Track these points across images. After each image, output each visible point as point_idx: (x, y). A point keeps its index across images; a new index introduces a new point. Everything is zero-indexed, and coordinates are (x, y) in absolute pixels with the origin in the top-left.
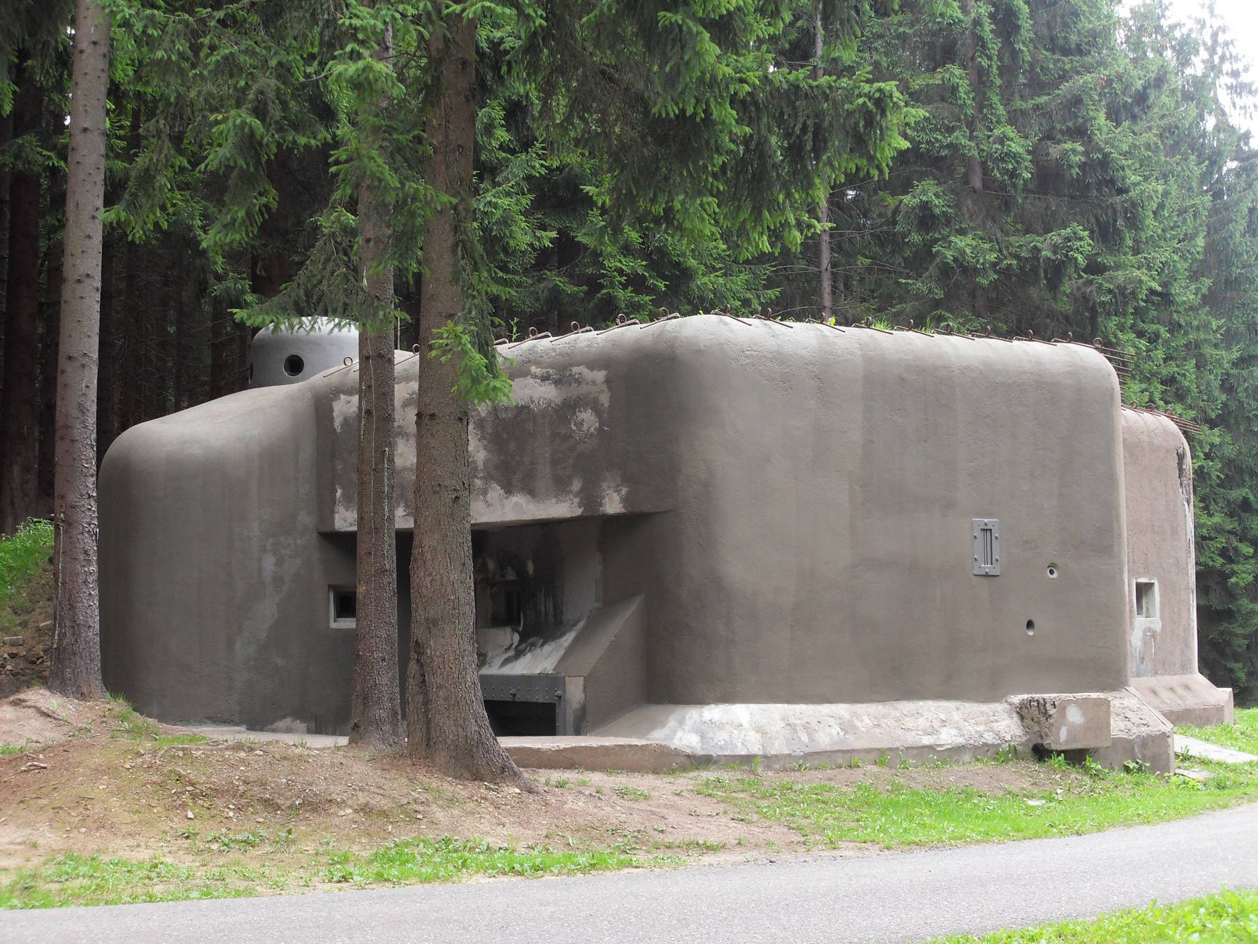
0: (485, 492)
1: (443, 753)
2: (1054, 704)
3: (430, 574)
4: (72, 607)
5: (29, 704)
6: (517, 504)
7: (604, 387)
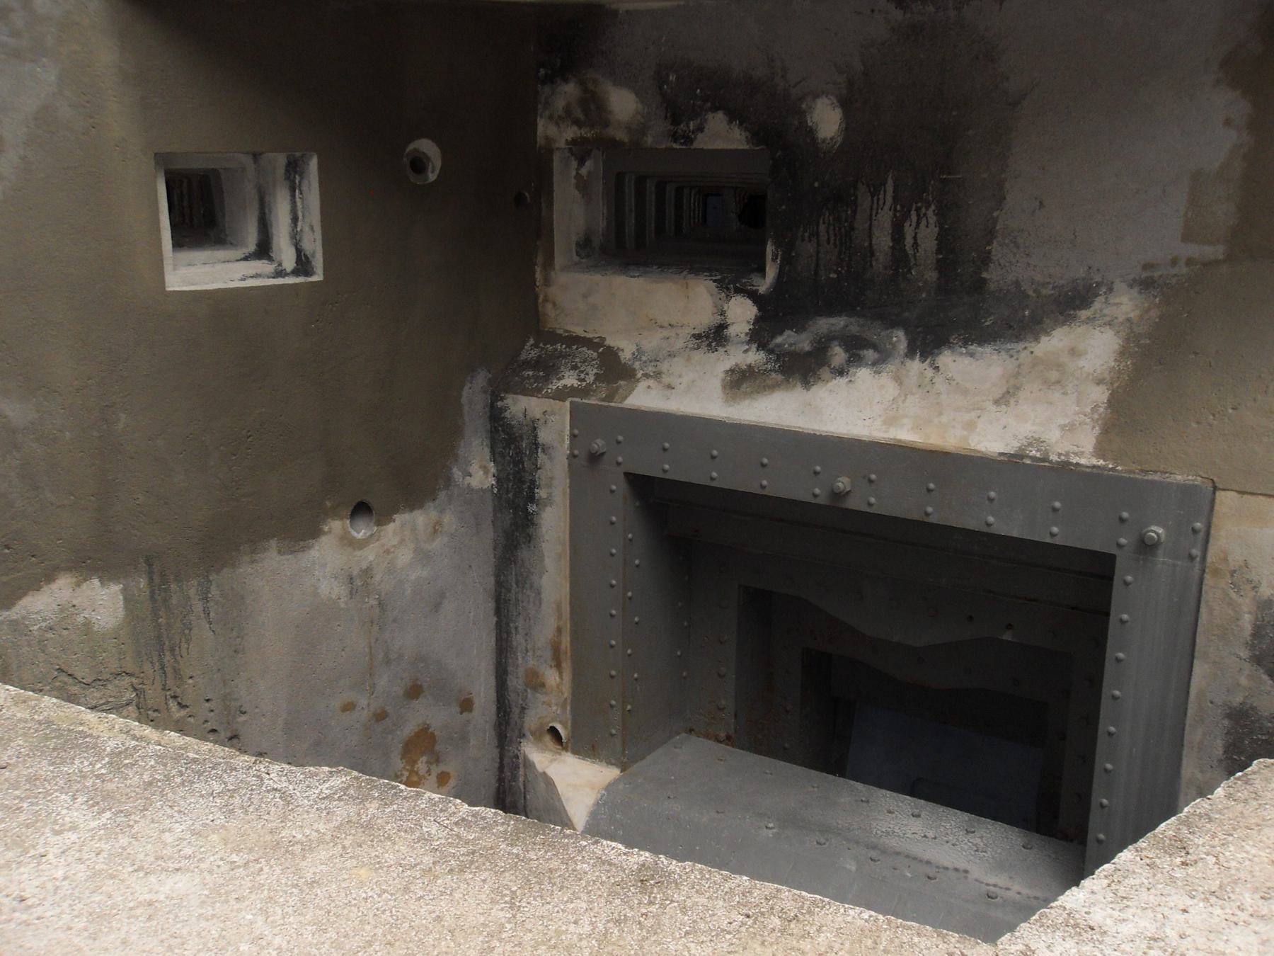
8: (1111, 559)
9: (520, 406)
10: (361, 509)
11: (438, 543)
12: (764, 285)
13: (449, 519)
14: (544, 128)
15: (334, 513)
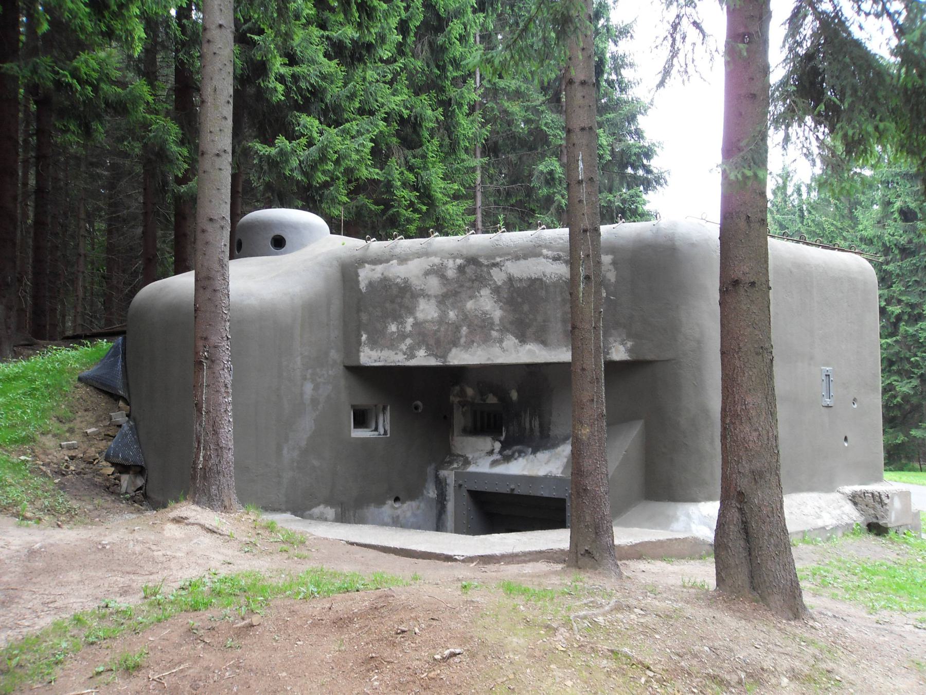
0: (501, 341)
1: (777, 597)
2: (888, 496)
3: (756, 430)
4: (216, 433)
5: (191, 521)
6: (529, 351)
7: (611, 267)
8: (563, 501)
9: (443, 473)
10: (397, 499)
11: (419, 512)
12: (502, 438)
13: (422, 505)
14: (452, 398)
15: (390, 498)
